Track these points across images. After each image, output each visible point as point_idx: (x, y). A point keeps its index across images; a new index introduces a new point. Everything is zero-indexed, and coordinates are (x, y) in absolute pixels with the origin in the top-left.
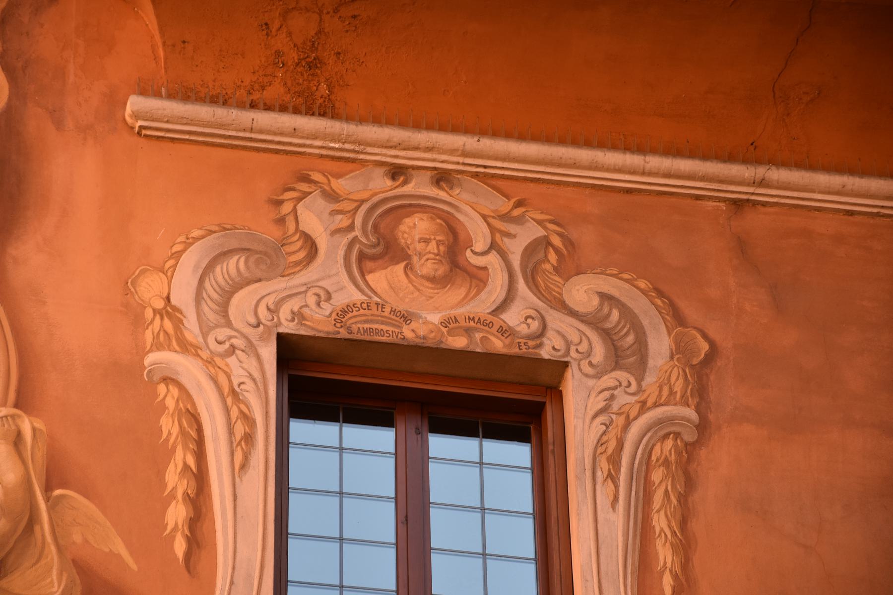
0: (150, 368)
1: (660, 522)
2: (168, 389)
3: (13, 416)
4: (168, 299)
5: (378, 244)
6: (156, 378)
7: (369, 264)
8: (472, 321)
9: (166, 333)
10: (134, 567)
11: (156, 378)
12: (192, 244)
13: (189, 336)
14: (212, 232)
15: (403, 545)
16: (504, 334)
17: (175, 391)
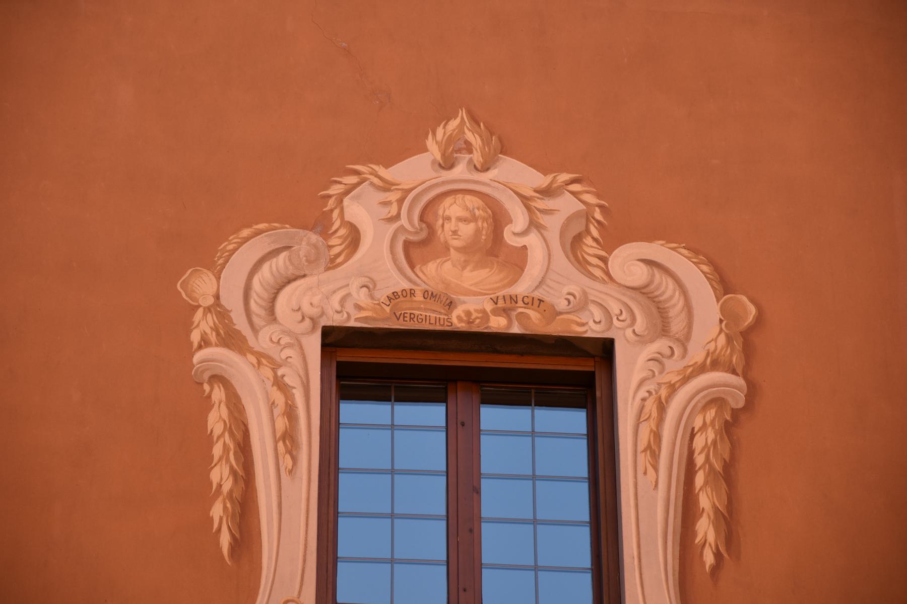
0: (198, 366)
1: (705, 501)
5: (421, 230)
7: (415, 253)
8: (433, 297)
16: (406, 319)
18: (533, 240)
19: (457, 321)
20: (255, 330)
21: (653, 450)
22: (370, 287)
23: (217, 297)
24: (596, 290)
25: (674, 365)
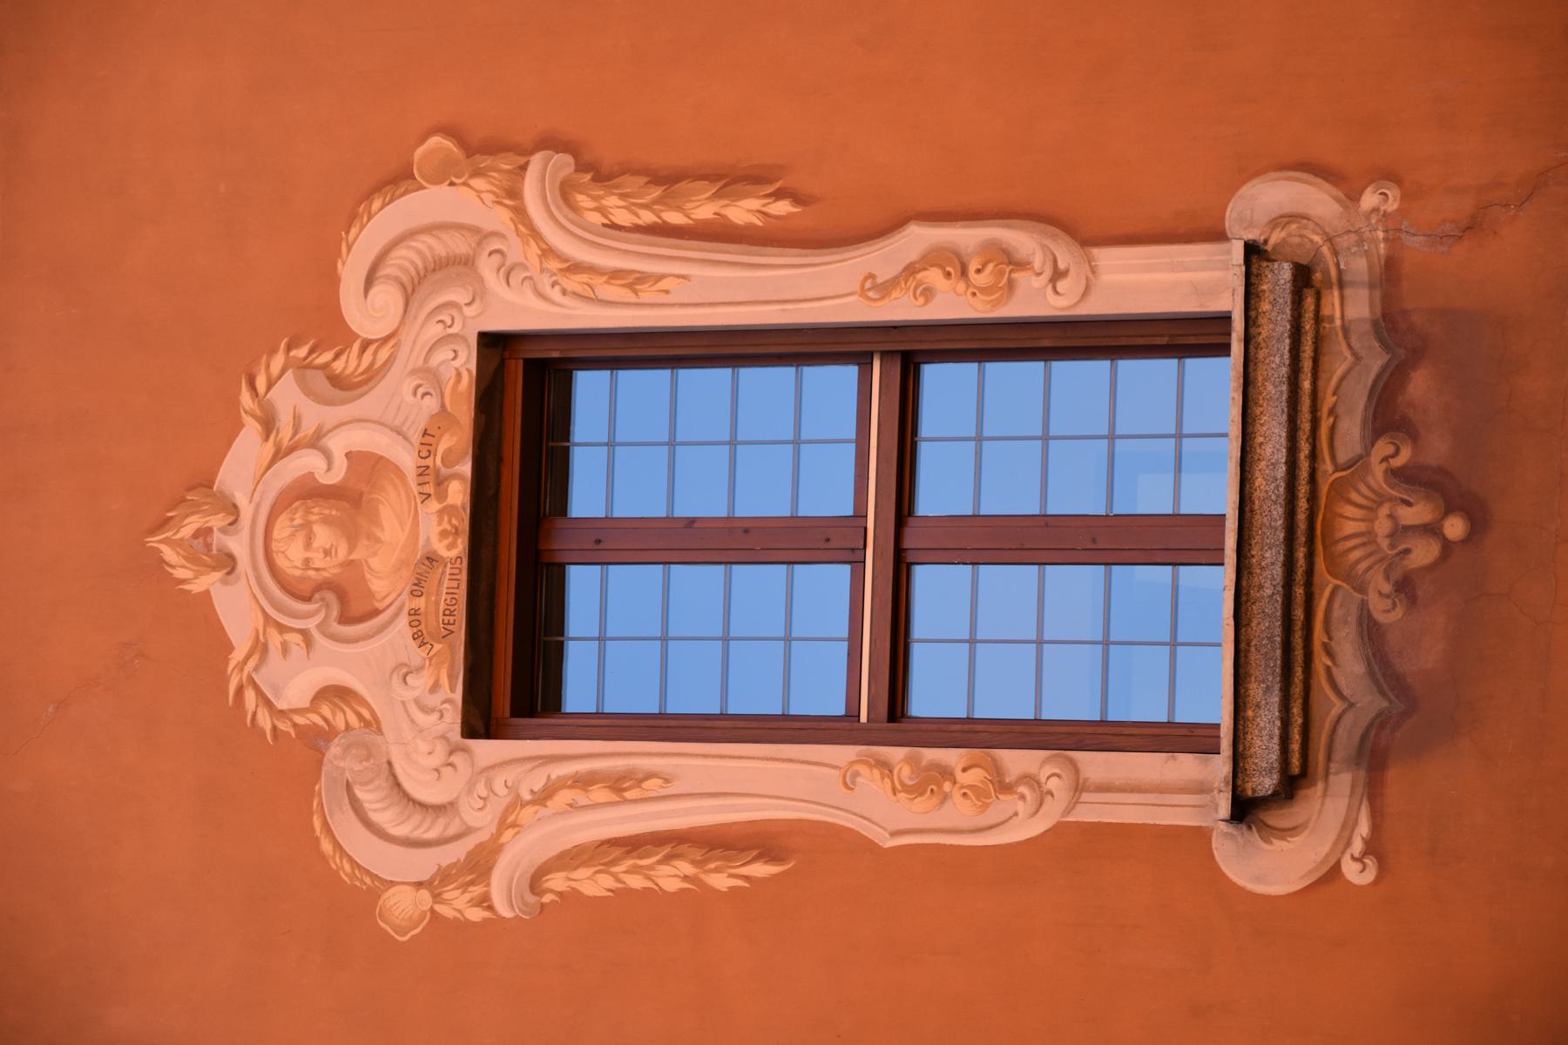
0: (517, 910)
1: (704, 211)
7: (357, 608)
15: (665, 556)
18: (339, 444)
19: (455, 550)
20: (467, 832)
21: (635, 280)
22: (406, 672)
23: (419, 885)
24: (409, 355)
25: (516, 249)
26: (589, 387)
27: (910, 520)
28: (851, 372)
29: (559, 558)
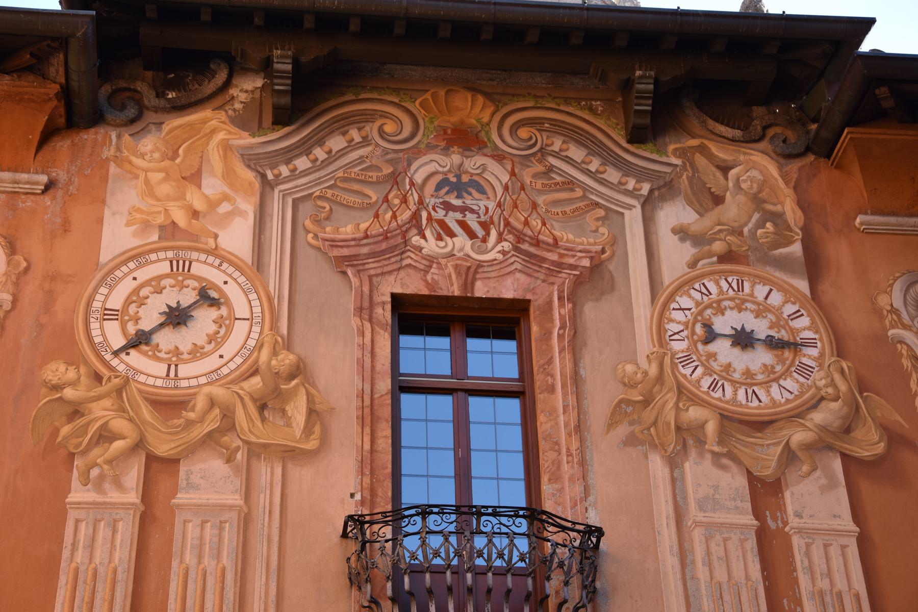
2: (902, 347)
3: (838, 361)
4: (892, 305)
6: (895, 341)
9: (895, 321)
10: (907, 426)
11: (895, 341)
12: (897, 280)
13: (905, 322)
14: (904, 274)
17: (905, 347)
26: (510, 346)
27: (467, 394)
28: (516, 376)
29: (452, 334)
